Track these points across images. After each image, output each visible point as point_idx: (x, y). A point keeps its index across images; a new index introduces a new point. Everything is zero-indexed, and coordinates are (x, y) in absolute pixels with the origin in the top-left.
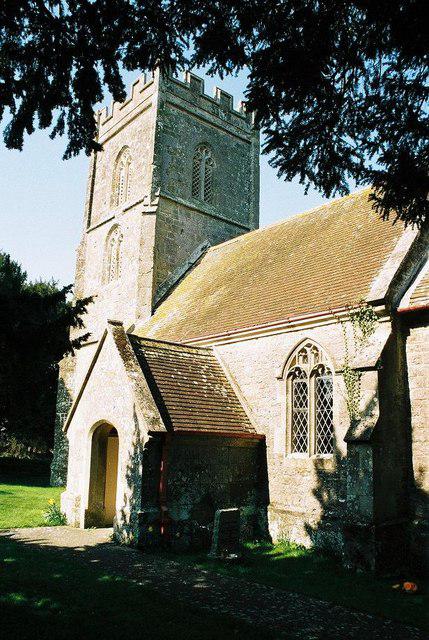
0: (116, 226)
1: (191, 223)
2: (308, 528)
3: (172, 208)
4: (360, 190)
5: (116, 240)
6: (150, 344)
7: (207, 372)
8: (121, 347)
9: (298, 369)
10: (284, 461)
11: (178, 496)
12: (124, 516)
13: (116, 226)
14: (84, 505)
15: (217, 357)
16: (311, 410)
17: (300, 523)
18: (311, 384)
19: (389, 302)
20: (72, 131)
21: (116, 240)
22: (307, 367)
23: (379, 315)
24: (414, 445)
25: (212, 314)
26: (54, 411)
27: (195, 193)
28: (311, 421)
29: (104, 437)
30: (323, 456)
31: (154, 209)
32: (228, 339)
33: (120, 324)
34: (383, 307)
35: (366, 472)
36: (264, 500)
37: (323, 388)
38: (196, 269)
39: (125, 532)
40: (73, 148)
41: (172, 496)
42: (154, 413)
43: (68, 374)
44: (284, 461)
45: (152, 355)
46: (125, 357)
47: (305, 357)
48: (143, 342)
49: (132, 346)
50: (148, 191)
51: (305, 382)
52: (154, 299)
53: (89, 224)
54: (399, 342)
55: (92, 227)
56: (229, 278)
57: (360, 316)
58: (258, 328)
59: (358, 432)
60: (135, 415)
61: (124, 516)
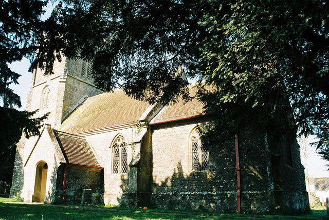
0: (47, 86)
1: (81, 87)
2: (118, 199)
3: (72, 80)
4: (118, 91)
5: (47, 91)
6: (61, 133)
7: (83, 145)
8: (50, 133)
9: (116, 144)
10: (110, 176)
11: (70, 187)
12: (49, 194)
13: (47, 86)
14: (32, 193)
15: (87, 140)
16: (120, 159)
17: (115, 197)
18: (121, 149)
19: (146, 121)
20: (46, 68)
21: (47, 91)
22: (119, 143)
23: (143, 126)
24: (153, 169)
25: (87, 124)
26: (13, 165)
27: (83, 74)
28: (120, 162)
29: (42, 167)
30: (124, 174)
31: (65, 80)
32: (91, 133)
33: (50, 125)
34: (144, 123)
35: (135, 175)
36: (102, 191)
37: (124, 150)
38: (81, 106)
39: (49, 199)
40: (46, 73)
41: (68, 187)
42: (62, 156)
43: (21, 149)
44: (110, 176)
45: (61, 137)
46: (52, 137)
47: (119, 140)
48: (58, 132)
49: (55, 134)
50: (63, 72)
51: (118, 147)
52: (62, 117)
53: (34, 84)
54: (150, 134)
55: (35, 85)
56: (94, 111)
57: (137, 125)
58: (102, 130)
59: (133, 163)
60: (55, 157)
61: (49, 194)
